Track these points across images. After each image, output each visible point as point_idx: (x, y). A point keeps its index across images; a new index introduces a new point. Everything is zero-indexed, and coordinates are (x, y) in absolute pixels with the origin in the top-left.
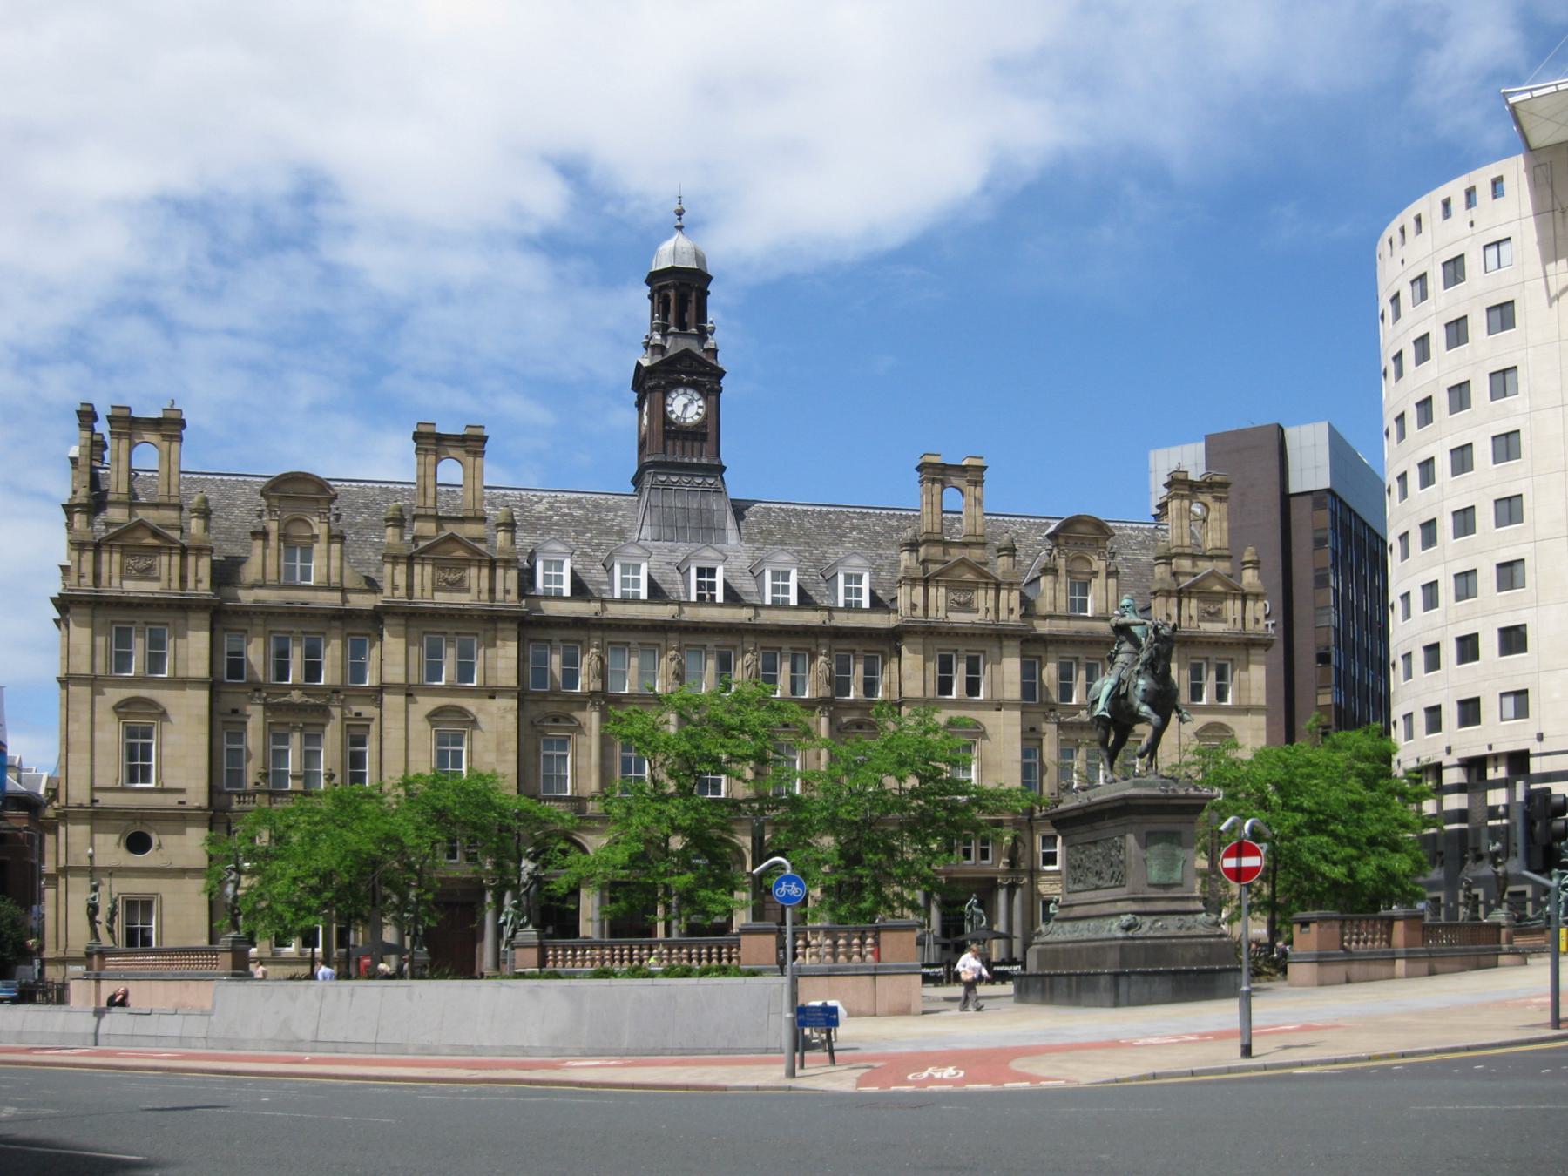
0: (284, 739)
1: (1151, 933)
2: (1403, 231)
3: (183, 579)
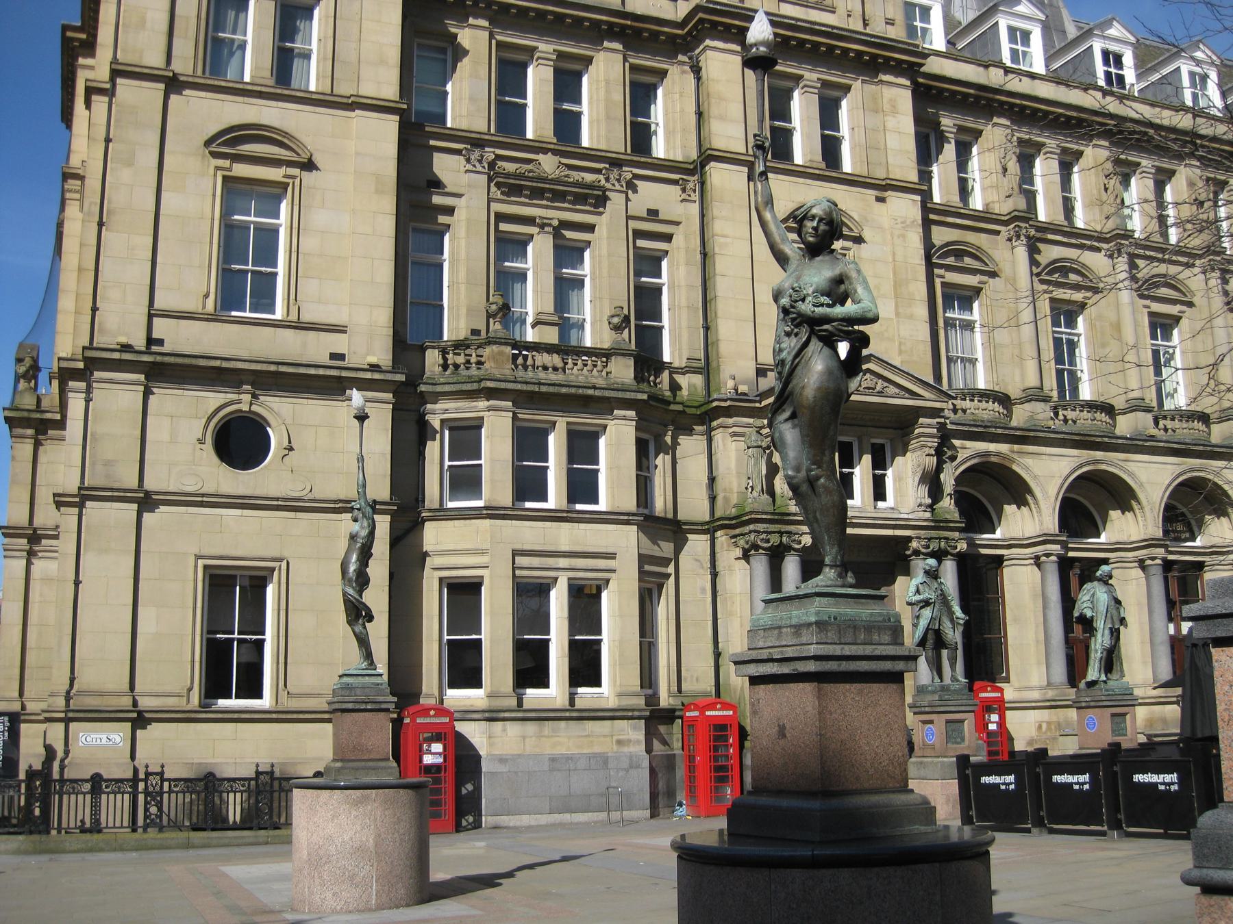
0: (517, 246)
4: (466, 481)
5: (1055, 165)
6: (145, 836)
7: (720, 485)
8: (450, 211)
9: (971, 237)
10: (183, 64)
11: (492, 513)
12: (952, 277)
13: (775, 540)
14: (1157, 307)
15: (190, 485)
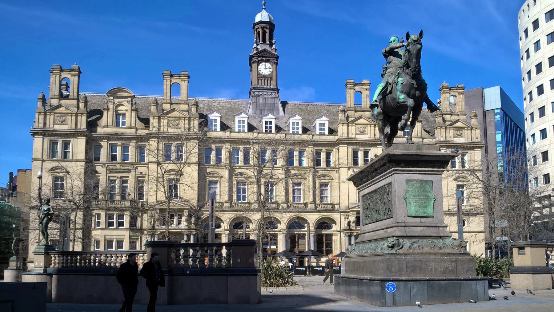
1: (411, 251)
2: (528, 6)
3: (76, 125)
6: (502, 260)
8: (99, 176)
10: (45, 157)
11: (101, 229)
12: (211, 179)
14: (459, 183)
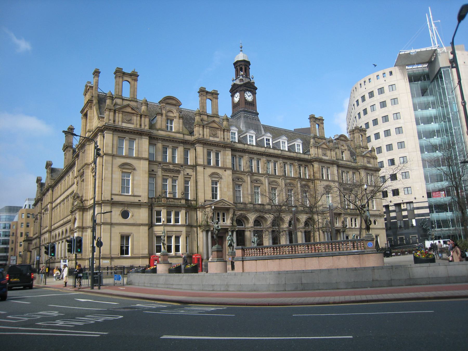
4: (159, 220)
5: (256, 161)
7: (198, 220)
9: (240, 176)
13: (207, 229)
15: (118, 222)
